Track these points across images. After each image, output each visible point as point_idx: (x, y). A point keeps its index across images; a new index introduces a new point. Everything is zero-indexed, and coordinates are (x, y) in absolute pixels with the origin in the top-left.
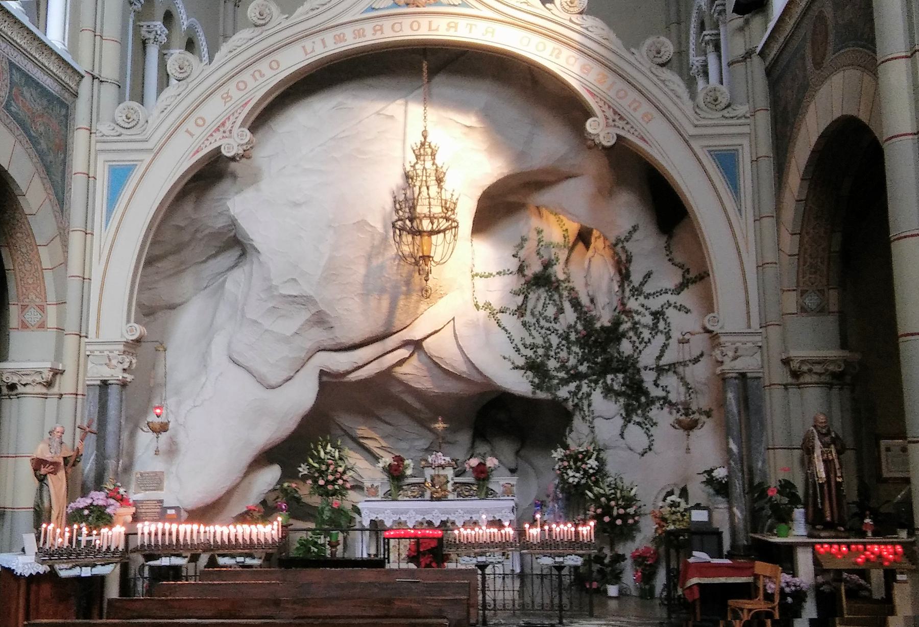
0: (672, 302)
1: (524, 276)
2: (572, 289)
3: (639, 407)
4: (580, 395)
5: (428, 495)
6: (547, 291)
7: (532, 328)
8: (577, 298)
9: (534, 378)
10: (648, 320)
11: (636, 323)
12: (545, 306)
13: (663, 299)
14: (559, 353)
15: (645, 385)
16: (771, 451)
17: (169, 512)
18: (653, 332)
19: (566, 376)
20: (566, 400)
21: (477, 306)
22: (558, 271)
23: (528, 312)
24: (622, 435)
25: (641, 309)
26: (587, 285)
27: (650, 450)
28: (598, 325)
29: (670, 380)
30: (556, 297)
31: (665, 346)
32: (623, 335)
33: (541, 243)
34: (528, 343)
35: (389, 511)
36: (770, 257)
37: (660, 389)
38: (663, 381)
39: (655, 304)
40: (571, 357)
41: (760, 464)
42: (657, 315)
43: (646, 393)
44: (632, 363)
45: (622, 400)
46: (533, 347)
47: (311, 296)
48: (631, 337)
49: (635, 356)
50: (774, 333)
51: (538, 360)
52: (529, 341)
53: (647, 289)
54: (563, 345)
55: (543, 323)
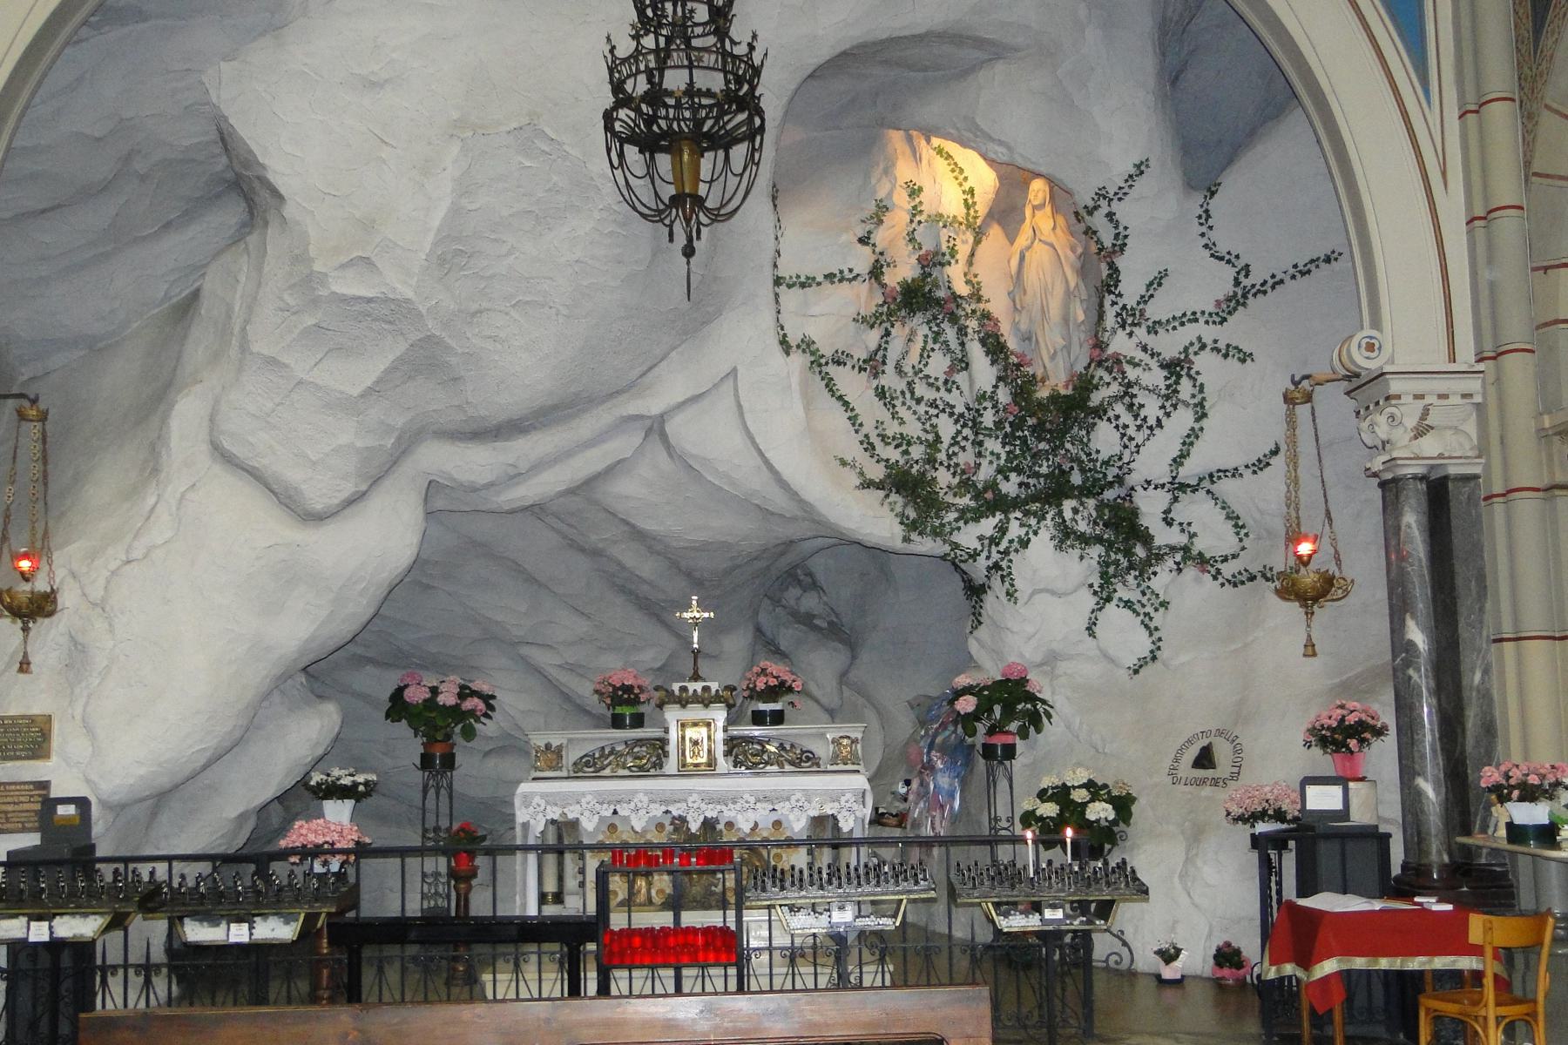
0: (1208, 340)
1: (884, 286)
2: (986, 316)
3: (1131, 567)
4: (1004, 545)
5: (671, 765)
6: (928, 323)
7: (898, 403)
8: (997, 336)
9: (905, 506)
10: (1157, 377)
11: (1130, 385)
12: (925, 354)
13: (1189, 333)
14: (955, 454)
15: (1144, 521)
16: (1508, 647)
17: (62, 810)
18: (1168, 404)
19: (973, 504)
20: (974, 555)
21: (784, 344)
22: (955, 276)
23: (890, 368)
24: (1090, 630)
25: (1139, 355)
26: (1016, 309)
27: (1154, 658)
28: (1043, 393)
29: (1198, 511)
30: (950, 334)
31: (1193, 435)
32: (1099, 412)
33: (918, 218)
34: (890, 433)
35: (589, 798)
36: (1507, 188)
37: (1176, 528)
38: (1180, 513)
39: (1170, 345)
40: (985, 462)
41: (1477, 677)
42: (1175, 368)
43: (1146, 539)
44: (1117, 476)
45: (1096, 551)
46: (903, 442)
47: (407, 301)
48: (1117, 417)
49: (1126, 459)
50: (1518, 370)
51: (914, 471)
52: (893, 429)
53: (1155, 311)
54: (966, 438)
55: (921, 389)
